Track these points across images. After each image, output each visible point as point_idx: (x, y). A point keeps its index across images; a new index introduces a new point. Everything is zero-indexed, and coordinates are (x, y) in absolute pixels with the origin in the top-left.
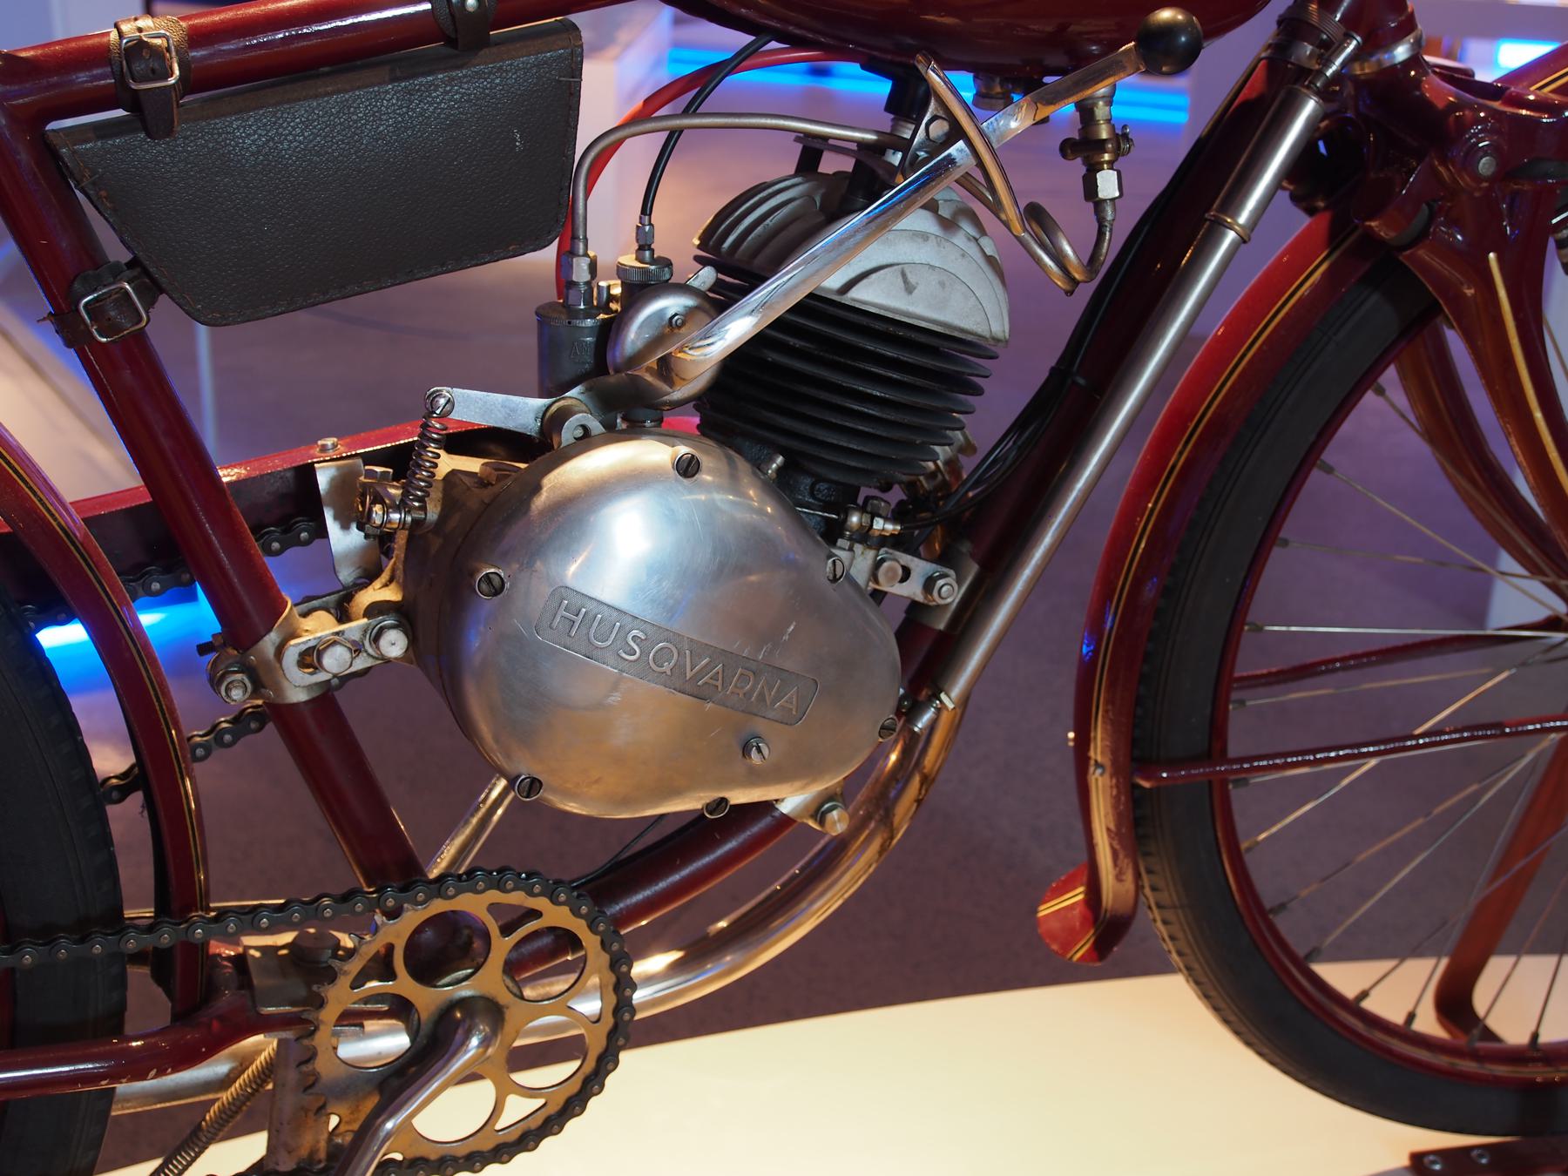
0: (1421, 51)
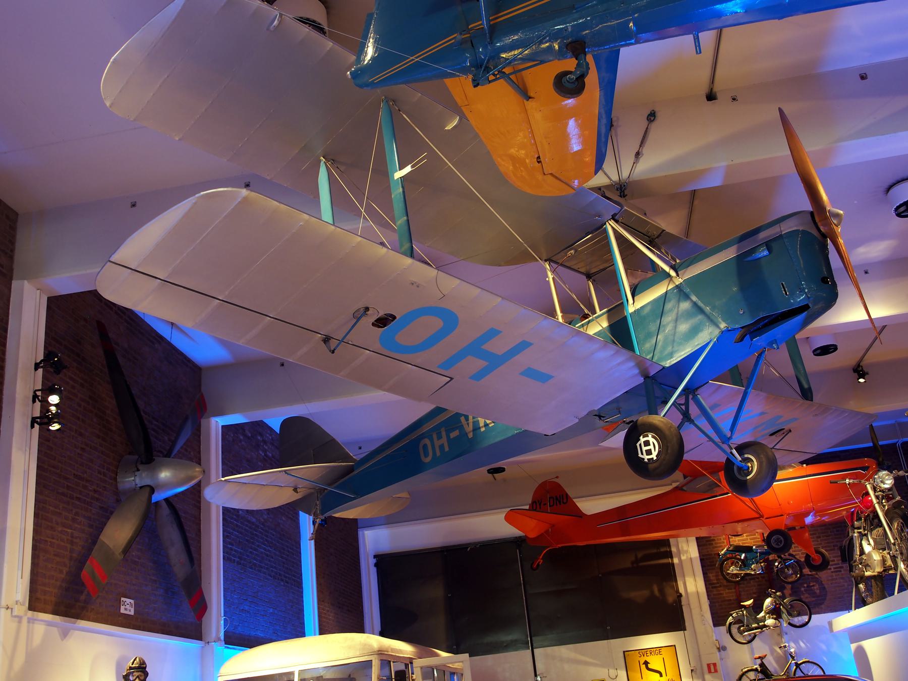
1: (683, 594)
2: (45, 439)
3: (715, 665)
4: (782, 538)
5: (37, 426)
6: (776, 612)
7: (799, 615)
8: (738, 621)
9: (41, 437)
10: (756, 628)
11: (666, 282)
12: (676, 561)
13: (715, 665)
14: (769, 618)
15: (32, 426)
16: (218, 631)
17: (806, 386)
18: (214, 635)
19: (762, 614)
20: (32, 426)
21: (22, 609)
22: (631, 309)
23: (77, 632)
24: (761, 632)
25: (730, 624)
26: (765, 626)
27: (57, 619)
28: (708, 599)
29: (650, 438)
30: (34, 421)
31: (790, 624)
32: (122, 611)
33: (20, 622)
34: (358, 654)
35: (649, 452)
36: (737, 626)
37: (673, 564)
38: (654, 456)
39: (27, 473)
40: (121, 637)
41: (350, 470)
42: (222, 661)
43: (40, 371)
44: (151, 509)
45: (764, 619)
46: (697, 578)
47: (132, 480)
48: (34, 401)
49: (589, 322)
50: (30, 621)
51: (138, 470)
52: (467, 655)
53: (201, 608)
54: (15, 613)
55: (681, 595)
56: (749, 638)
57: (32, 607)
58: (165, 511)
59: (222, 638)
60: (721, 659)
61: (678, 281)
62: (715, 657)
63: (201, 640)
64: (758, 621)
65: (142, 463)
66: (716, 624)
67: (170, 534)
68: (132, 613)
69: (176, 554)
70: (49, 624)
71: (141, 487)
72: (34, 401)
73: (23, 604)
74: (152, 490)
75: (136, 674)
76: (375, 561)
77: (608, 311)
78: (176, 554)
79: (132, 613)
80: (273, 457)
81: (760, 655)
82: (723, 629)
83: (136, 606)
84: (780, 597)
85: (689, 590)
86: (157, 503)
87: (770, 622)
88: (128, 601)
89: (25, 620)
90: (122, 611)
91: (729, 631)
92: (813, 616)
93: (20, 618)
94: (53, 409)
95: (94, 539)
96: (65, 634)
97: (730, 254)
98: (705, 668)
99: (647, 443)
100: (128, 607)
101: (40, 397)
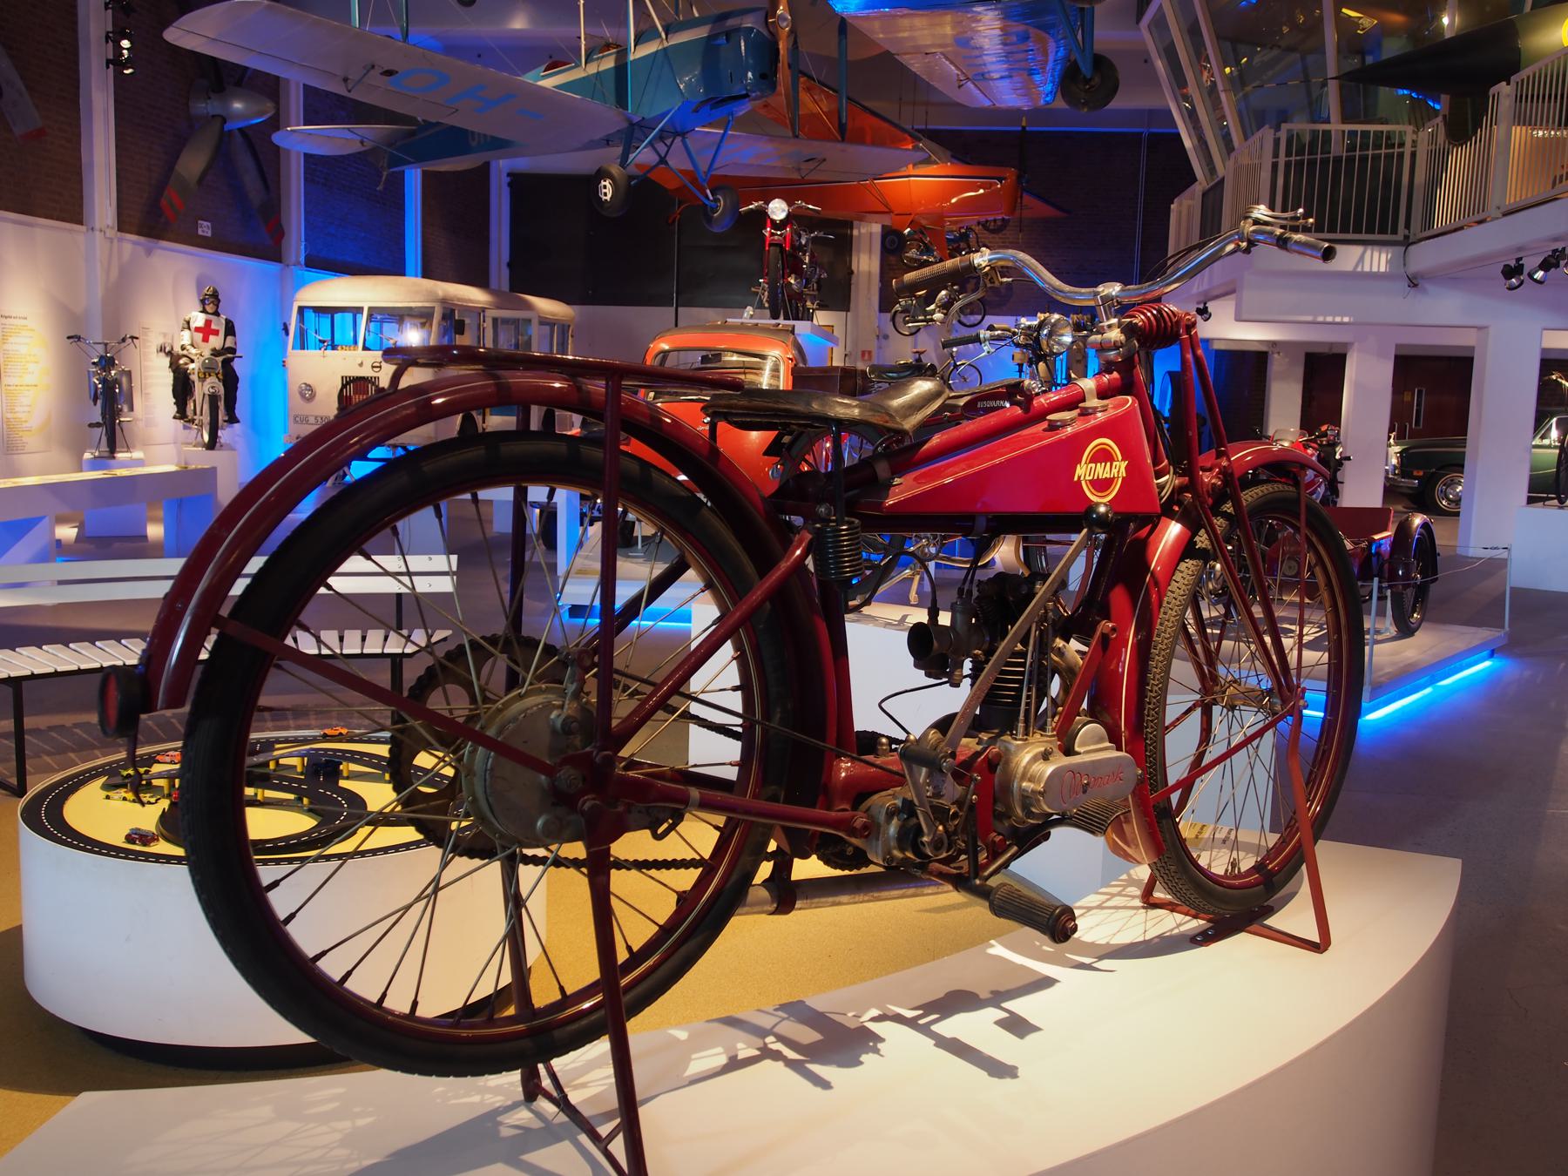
0: (1356, 344)
1: (855, 271)
2: (119, 79)
3: (870, 352)
4: (896, 240)
5: (110, 44)
6: (946, 306)
7: (972, 313)
8: (905, 310)
9: (115, 77)
10: (922, 321)
11: (658, 41)
12: (855, 232)
13: (870, 352)
14: (939, 312)
15: (108, 67)
16: (298, 256)
17: (844, 121)
18: (293, 259)
19: (933, 307)
20: (108, 67)
21: (112, 233)
22: (631, 57)
23: (160, 251)
24: (925, 326)
25: (896, 312)
26: (932, 320)
27: (142, 239)
28: (881, 281)
29: (607, 183)
30: (108, 62)
31: (960, 322)
32: (200, 232)
33: (112, 242)
34: (422, 299)
35: (605, 194)
36: (904, 315)
37: (852, 236)
38: (608, 198)
39: (106, 112)
40: (196, 255)
41: (412, 134)
42: (302, 284)
43: (110, 11)
44: (224, 139)
45: (933, 312)
46: (873, 257)
47: (204, 107)
48: (107, 42)
49: (603, 57)
50: (120, 240)
51: (210, 98)
52: (933, 1042)
53: (278, 234)
54: (108, 235)
55: (852, 272)
56: (914, 330)
57: (119, 230)
58: (239, 138)
59: (303, 262)
60: (880, 348)
61: (666, 44)
62: (872, 345)
63: (280, 262)
64: (926, 313)
65: (213, 91)
66: (881, 310)
67: (245, 161)
68: (209, 234)
69: (251, 181)
70: (135, 243)
71: (213, 116)
72: (107, 42)
73: (113, 228)
74: (224, 121)
75: (211, 300)
76: (508, 179)
77: (618, 52)
78: (251, 181)
79: (209, 234)
80: (192, 345)
81: (920, 350)
82: (889, 316)
83: (213, 228)
84: (956, 291)
85: (861, 269)
86: (230, 131)
87: (938, 316)
88: (205, 223)
89: (116, 241)
90: (200, 232)
91: (893, 319)
92: (987, 317)
93: (111, 240)
94: (125, 52)
95: (170, 167)
96: (149, 252)
97: (702, 32)
98: (860, 353)
99: (605, 187)
100: (205, 229)
101: (114, 38)
